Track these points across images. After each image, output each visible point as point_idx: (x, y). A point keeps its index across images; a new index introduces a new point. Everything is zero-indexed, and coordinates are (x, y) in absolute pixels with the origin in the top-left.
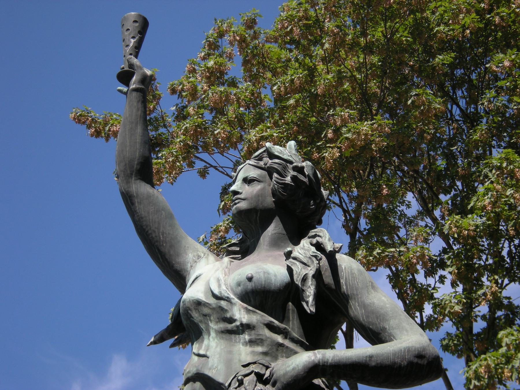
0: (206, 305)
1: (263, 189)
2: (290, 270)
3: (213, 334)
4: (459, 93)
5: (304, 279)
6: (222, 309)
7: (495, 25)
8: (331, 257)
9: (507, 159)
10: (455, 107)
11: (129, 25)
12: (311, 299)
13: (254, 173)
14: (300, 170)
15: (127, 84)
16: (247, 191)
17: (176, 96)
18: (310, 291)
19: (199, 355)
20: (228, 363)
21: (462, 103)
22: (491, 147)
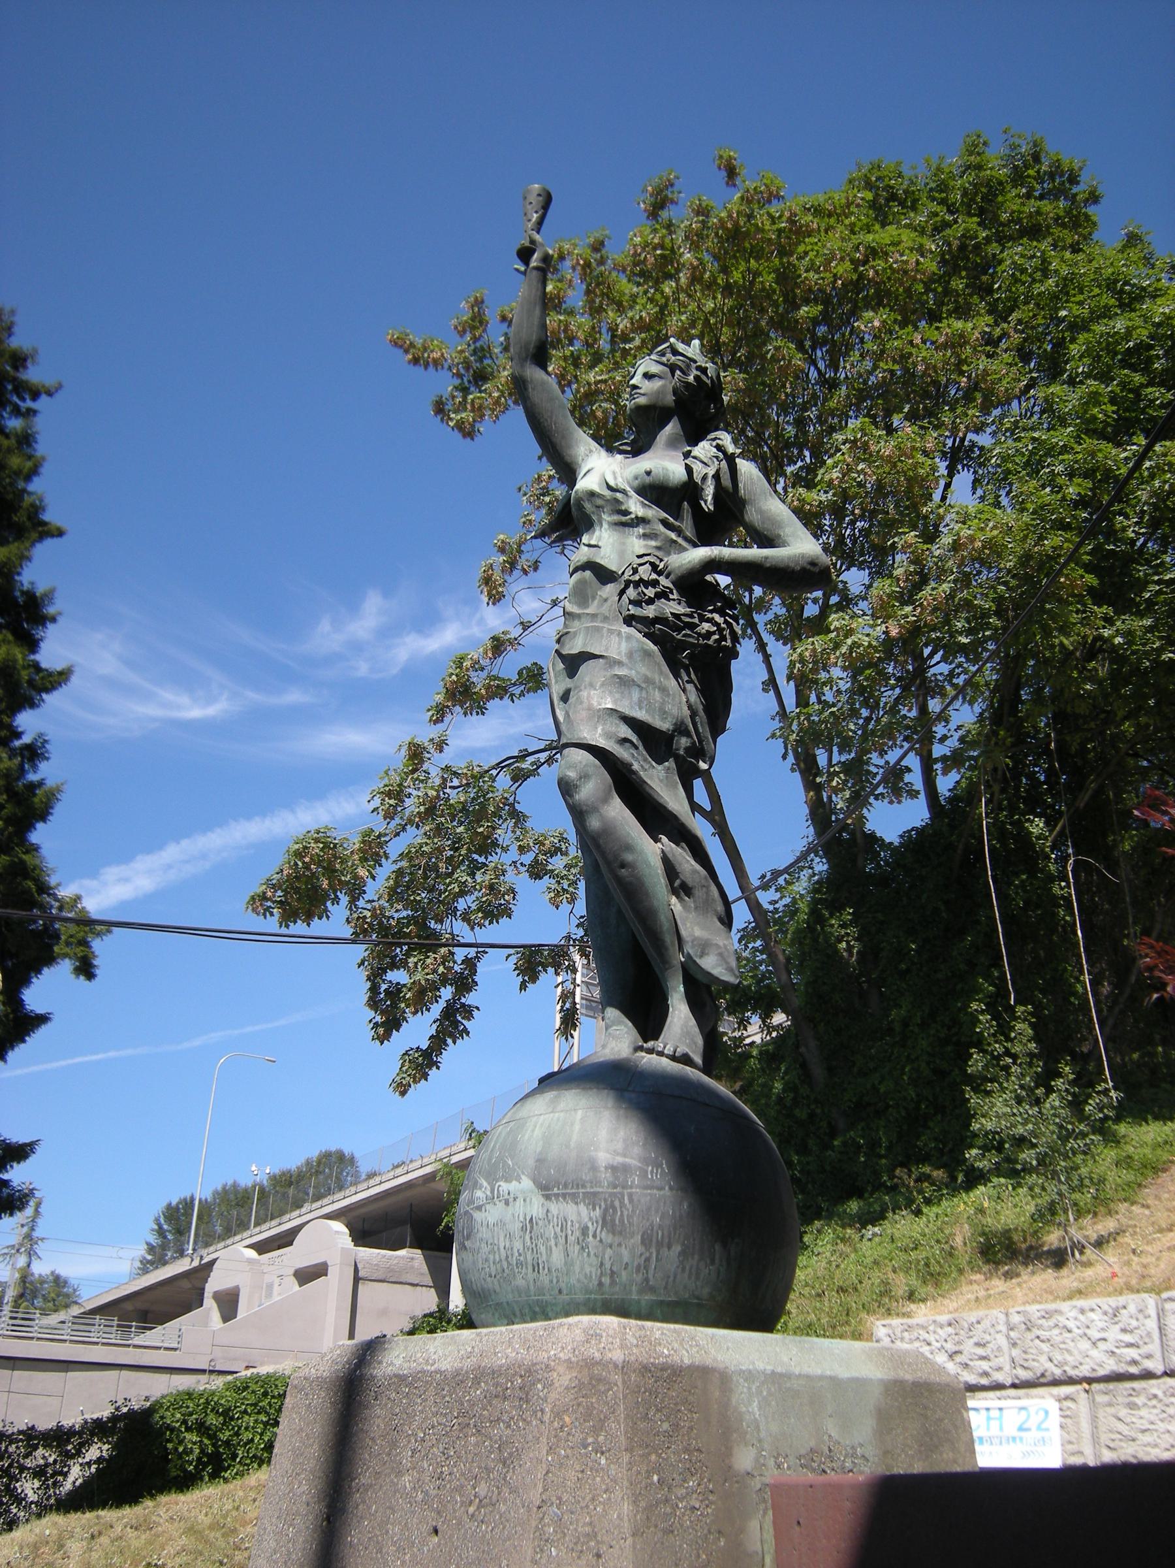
0: (599, 496)
1: (664, 386)
2: (689, 469)
3: (605, 525)
4: (819, 354)
5: (704, 478)
6: (617, 501)
7: (869, 280)
8: (730, 459)
9: (862, 430)
10: (812, 368)
11: (533, 198)
12: (710, 498)
13: (655, 369)
14: (704, 370)
15: (526, 262)
16: (647, 386)
17: (506, 324)
18: (709, 491)
19: (589, 546)
20: (622, 554)
21: (821, 365)
22: (848, 417)
